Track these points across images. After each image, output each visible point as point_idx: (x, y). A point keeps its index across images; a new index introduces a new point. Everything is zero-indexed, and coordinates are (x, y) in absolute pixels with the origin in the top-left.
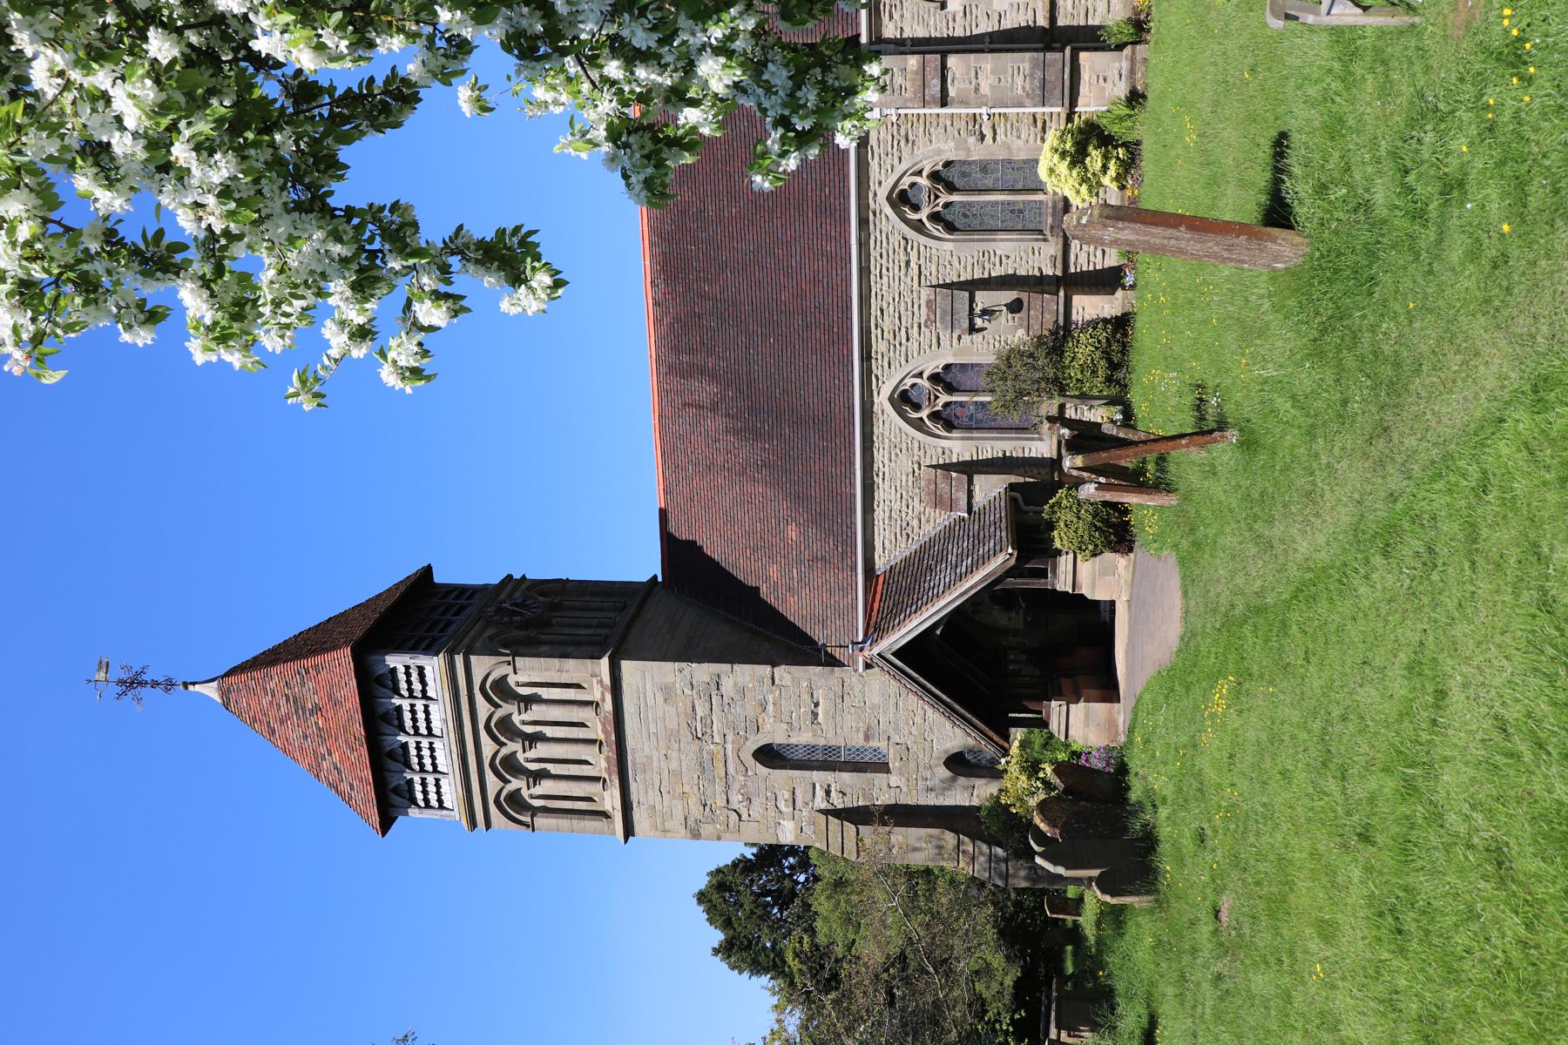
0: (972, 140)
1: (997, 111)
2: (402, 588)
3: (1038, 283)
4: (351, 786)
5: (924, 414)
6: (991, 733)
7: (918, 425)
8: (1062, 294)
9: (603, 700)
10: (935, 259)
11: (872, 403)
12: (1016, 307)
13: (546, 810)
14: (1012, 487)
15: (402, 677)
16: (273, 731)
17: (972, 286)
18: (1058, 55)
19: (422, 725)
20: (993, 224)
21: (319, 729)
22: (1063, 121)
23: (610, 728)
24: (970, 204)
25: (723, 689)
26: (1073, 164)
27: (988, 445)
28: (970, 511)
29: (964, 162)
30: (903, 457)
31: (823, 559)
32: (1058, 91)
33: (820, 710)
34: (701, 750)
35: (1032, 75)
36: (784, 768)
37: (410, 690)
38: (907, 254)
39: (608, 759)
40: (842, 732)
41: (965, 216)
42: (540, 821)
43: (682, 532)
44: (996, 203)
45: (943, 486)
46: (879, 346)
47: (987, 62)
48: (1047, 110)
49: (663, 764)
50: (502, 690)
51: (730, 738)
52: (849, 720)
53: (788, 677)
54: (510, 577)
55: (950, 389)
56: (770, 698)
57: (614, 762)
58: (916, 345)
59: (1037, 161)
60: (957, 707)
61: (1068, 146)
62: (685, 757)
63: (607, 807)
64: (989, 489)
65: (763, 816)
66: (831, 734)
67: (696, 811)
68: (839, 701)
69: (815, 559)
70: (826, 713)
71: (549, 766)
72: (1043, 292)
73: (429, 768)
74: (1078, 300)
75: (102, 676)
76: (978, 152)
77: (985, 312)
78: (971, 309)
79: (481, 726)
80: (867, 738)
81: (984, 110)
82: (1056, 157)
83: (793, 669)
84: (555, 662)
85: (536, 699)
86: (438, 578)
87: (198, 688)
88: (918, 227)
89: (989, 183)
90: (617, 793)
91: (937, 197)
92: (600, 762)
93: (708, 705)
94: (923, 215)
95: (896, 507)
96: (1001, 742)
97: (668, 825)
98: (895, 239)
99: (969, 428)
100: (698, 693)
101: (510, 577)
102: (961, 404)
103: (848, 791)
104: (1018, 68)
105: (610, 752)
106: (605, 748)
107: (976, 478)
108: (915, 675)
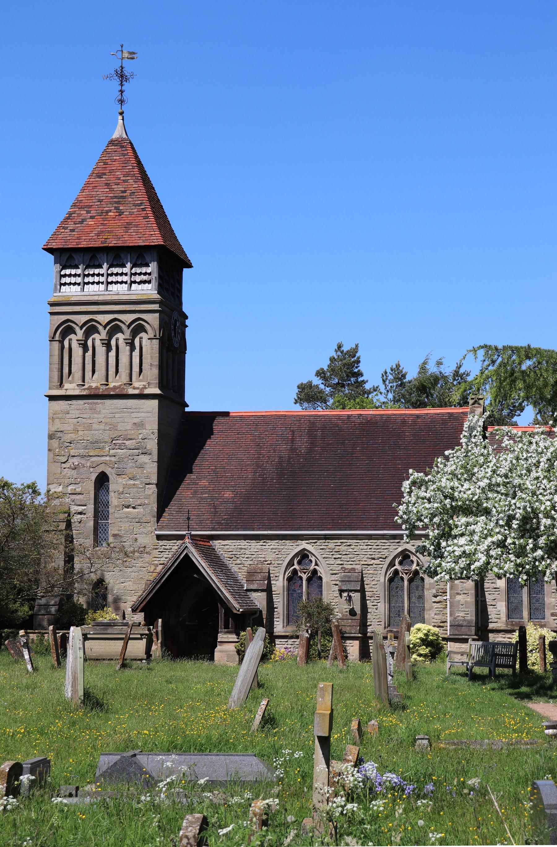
0: (434, 591)
1: (448, 603)
2: (178, 253)
3: (364, 625)
5: (296, 566)
6: (144, 603)
7: (291, 563)
8: (360, 635)
9: (134, 388)
10: (376, 572)
11: (302, 540)
12: (352, 612)
13: (63, 347)
14: (261, 612)
15: (144, 270)
17: (362, 591)
18: (473, 633)
20: (393, 602)
21: (107, 212)
23: (117, 391)
25: (143, 456)
26: (422, 639)
27: (281, 600)
28: (247, 590)
30: (274, 555)
31: (216, 512)
32: (457, 633)
33: (131, 510)
34: (106, 442)
35: (465, 620)
36: (95, 489)
38: (378, 559)
39: (97, 388)
40: (118, 522)
41: (397, 588)
42: (56, 345)
43: (218, 425)
44: (403, 603)
45: (259, 577)
46: (332, 544)
47: (471, 599)
48: (448, 628)
49: (95, 420)
51: (113, 459)
52: (125, 526)
53: (150, 492)
54: (186, 317)
55: (309, 580)
56: (137, 482)
57: (96, 392)
58: (332, 563)
59: (424, 623)
60: (159, 586)
61: (431, 637)
62: (100, 432)
63: (66, 386)
64: (259, 600)
65: (64, 476)
66: (117, 515)
68: (137, 520)
69: (215, 507)
70: (129, 513)
74: (356, 643)
77: (350, 597)
78: (351, 591)
81: (448, 597)
82: (426, 632)
83: (155, 495)
84: (156, 362)
85: (133, 348)
88: (392, 564)
89: (413, 599)
90: (77, 392)
91: (406, 574)
92: (95, 382)
93: (132, 447)
94: (397, 567)
95: (247, 552)
96: (140, 608)
97: (57, 421)
98: (386, 553)
99: (288, 590)
101: (186, 317)
102: (301, 585)
103: (82, 525)
104: (467, 613)
105: (102, 390)
106: (104, 387)
107: (265, 593)
108: (176, 564)
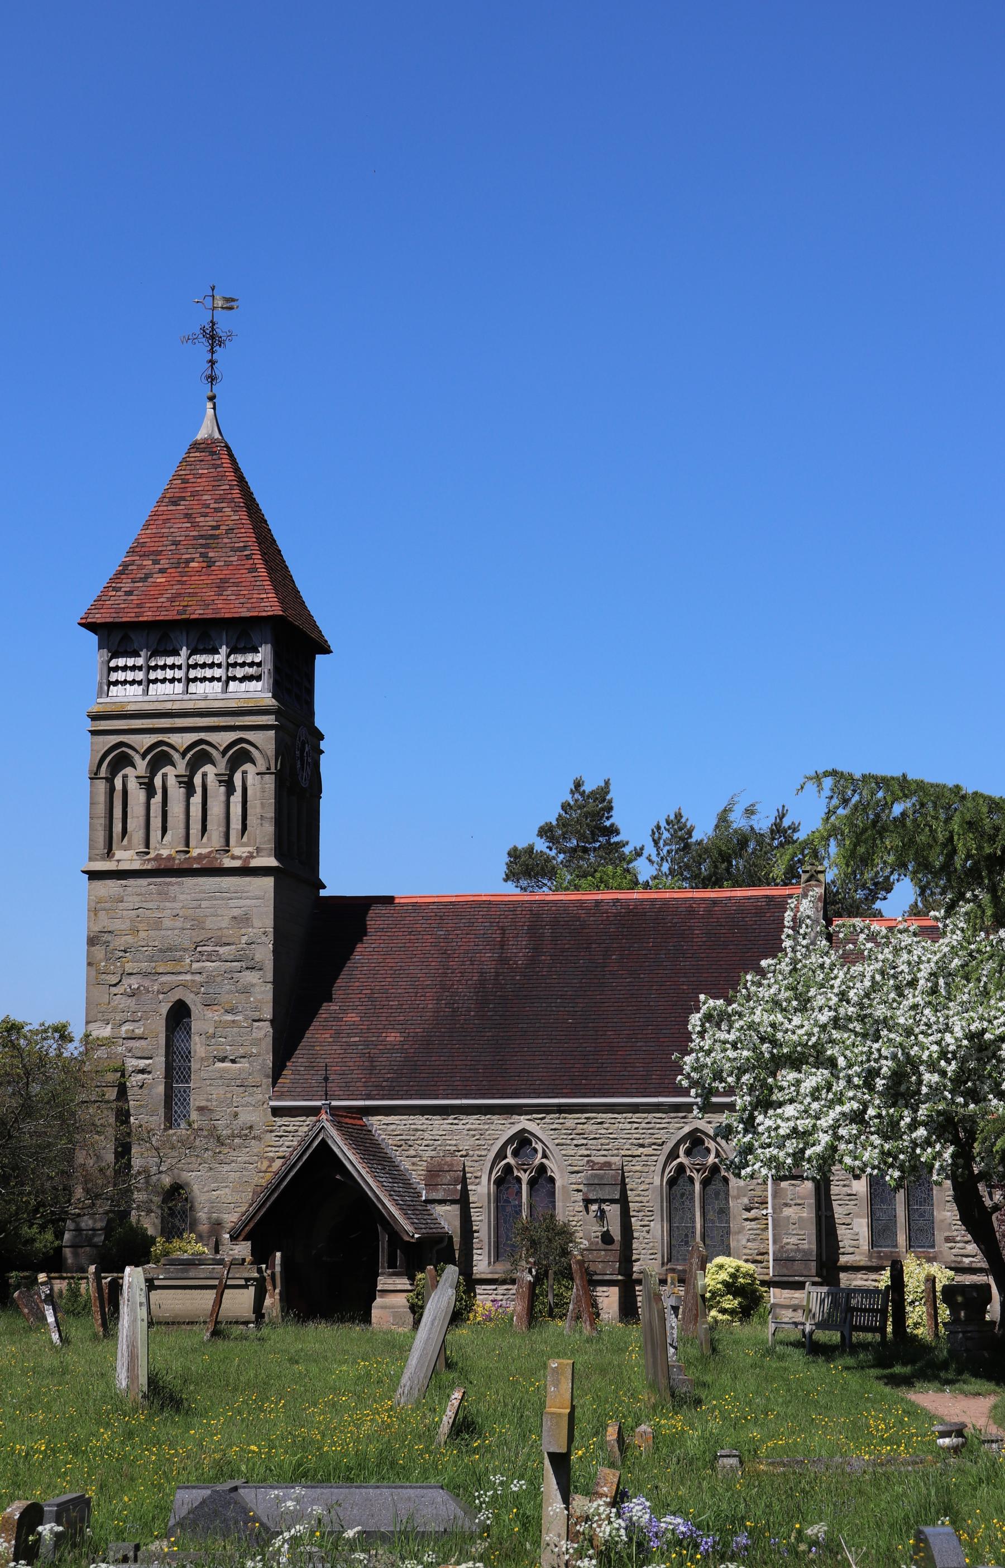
0: (746, 1201)
1: (770, 1218)
3: (626, 1259)
4: (129, 593)
6: (252, 1225)
7: (501, 1155)
8: (620, 1277)
9: (233, 857)
11: (521, 1115)
12: (607, 1238)
13: (112, 789)
14: (451, 1238)
16: (175, 503)
17: (623, 1201)
18: (814, 1272)
19: (198, 673)
22: (762, 1277)
24: (692, 1199)
25: (247, 973)
26: (724, 1283)
27: (484, 1217)
28: (428, 1201)
29: (727, 1193)
32: (785, 1272)
33: (227, 1065)
34: (185, 950)
35: (798, 1250)
37: (235, 665)
38: (650, 1145)
39: (170, 858)
40: (206, 1086)
41: (683, 1195)
42: (102, 786)
43: (374, 919)
44: (694, 1222)
46: (571, 1120)
47: (808, 1213)
50: (239, 757)
51: (198, 978)
52: (218, 1092)
53: (261, 1034)
55: (532, 1183)
56: (239, 1018)
57: (169, 865)
58: (572, 1153)
59: (729, 1255)
62: (175, 933)
63: (119, 854)
64: (447, 1218)
66: (203, 1074)
67: (120, 942)
68: (238, 1082)
69: (371, 1059)
71: (158, 798)
72: (619, 1261)
73: (152, 676)
75: (219, 303)
76: (736, 1205)
77: (603, 1212)
78: (604, 1201)
79: (202, 735)
80: (201, 1109)
81: (770, 1210)
82: (733, 1270)
83: (269, 1040)
86: (320, 659)
87: (210, 412)
88: (673, 1155)
89: (711, 1215)
90: (136, 865)
91: (698, 1171)
92: (166, 848)
93: (231, 957)
94: (682, 1159)
95: (426, 1135)
97: (102, 914)
98: (662, 1135)
99: (497, 1200)
100: (243, 949)
102: (519, 1192)
103: (145, 1091)
104: (803, 1239)
106: (183, 856)
107: (457, 1207)
108: (305, 1158)
